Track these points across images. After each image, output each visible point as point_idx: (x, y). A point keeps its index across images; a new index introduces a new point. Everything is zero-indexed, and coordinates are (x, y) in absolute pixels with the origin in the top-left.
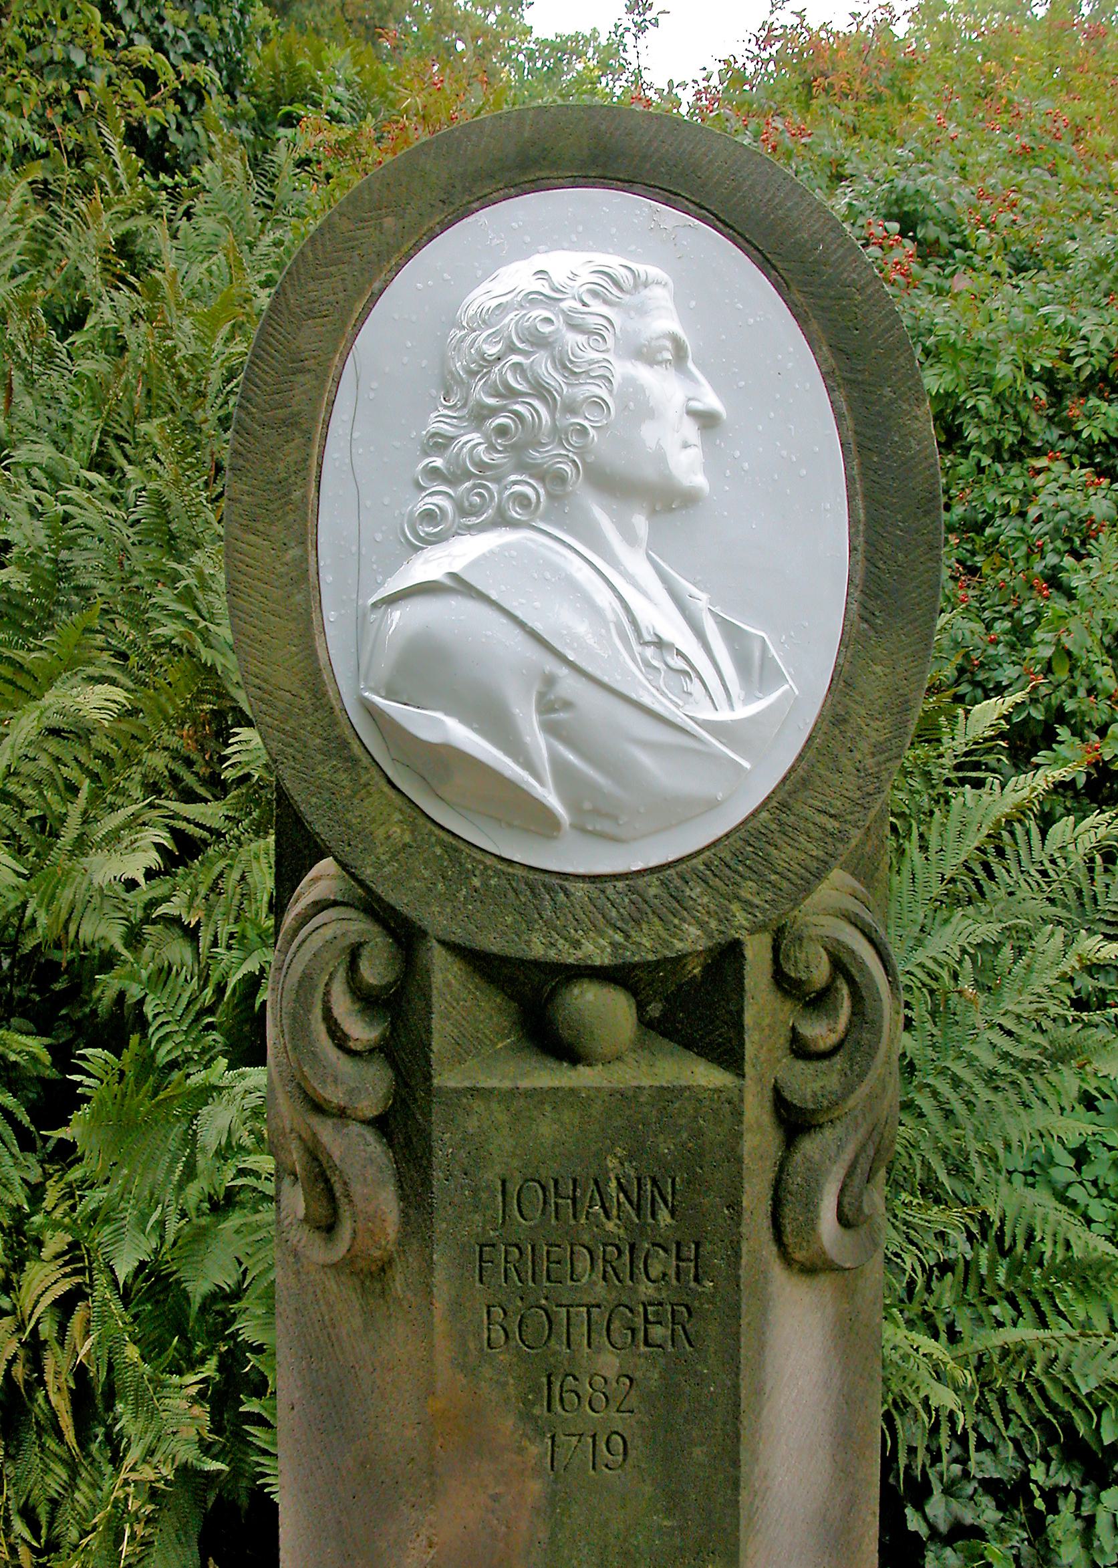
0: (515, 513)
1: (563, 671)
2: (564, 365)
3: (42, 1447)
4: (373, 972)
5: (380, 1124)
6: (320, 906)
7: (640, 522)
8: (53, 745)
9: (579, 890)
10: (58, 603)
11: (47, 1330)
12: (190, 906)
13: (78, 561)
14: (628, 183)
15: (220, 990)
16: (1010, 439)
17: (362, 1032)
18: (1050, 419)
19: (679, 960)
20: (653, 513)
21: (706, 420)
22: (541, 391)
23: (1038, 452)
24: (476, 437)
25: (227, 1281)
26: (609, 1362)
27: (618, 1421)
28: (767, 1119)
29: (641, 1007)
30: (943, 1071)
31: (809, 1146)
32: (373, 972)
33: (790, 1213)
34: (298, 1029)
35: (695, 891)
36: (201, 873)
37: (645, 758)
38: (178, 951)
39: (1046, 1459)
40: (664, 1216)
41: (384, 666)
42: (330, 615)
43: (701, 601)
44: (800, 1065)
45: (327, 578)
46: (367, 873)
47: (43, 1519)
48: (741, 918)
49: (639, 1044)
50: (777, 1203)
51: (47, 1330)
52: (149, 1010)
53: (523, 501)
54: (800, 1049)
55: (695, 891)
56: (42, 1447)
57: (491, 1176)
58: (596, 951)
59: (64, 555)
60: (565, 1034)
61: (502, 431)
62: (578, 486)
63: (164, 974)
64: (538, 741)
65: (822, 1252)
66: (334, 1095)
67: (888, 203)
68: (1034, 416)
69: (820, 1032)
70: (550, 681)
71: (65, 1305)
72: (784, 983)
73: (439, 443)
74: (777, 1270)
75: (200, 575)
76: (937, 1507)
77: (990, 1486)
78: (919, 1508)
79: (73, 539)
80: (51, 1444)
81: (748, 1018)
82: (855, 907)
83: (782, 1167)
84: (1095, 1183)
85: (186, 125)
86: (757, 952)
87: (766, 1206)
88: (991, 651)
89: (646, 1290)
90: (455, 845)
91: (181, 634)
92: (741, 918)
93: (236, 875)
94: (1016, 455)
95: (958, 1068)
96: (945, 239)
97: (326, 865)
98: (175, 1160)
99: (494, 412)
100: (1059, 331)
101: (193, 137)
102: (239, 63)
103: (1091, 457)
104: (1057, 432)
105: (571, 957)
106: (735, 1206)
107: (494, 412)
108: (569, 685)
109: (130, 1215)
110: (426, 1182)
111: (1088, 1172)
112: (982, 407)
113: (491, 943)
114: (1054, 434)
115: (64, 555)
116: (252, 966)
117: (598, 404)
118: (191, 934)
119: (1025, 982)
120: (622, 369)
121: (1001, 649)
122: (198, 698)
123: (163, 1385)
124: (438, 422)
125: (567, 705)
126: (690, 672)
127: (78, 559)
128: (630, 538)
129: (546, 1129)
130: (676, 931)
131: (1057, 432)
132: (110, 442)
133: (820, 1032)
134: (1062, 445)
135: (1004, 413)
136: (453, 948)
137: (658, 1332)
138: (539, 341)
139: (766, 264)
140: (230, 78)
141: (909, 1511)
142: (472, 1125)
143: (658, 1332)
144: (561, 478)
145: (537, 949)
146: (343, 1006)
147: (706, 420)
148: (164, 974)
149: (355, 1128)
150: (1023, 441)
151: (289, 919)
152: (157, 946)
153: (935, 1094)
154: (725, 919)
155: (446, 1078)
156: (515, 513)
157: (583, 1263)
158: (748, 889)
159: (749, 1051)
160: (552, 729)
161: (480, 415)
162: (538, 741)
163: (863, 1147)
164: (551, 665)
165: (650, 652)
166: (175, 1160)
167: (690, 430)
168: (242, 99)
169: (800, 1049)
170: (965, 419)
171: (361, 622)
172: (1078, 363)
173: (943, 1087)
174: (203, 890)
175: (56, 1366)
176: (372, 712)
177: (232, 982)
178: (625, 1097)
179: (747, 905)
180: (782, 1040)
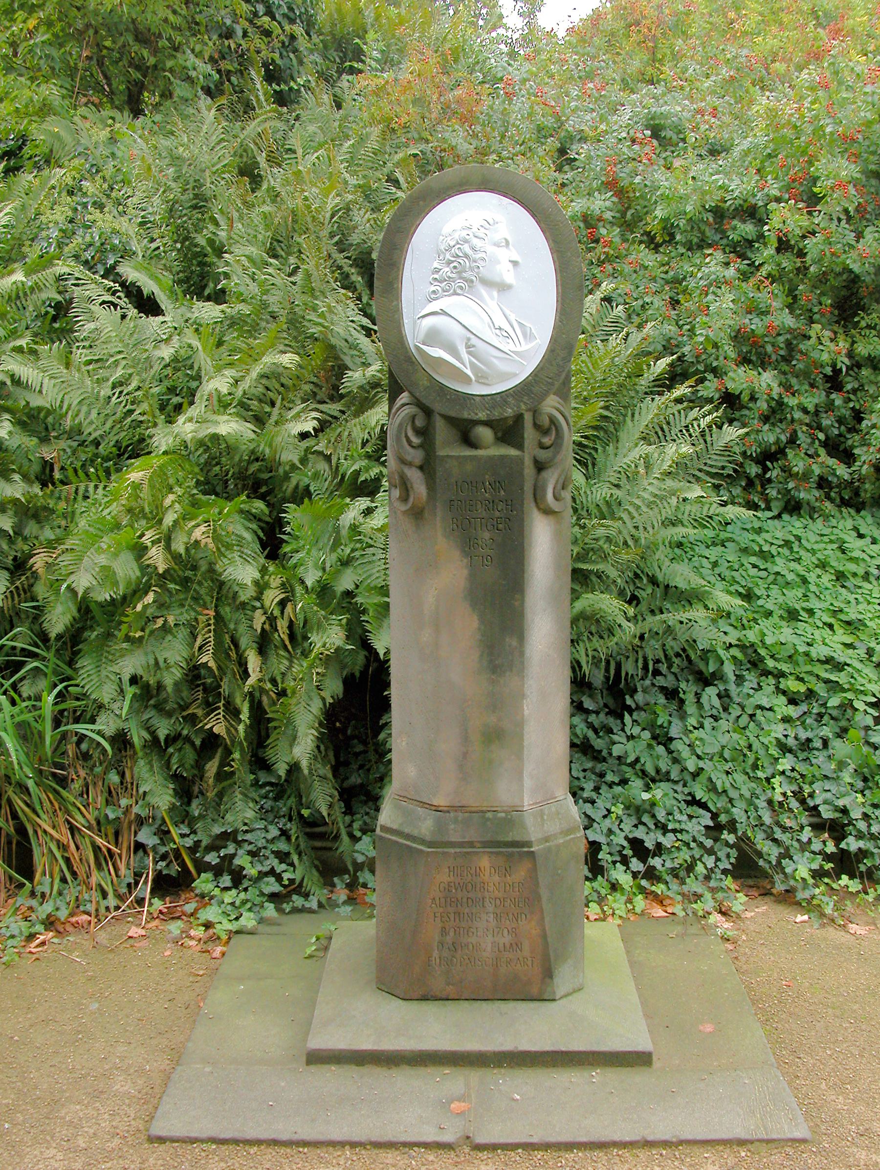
0: (459, 291)
1: (472, 337)
2: (473, 249)
3: (278, 654)
4: (419, 423)
5: (421, 468)
6: (403, 405)
7: (495, 294)
8: (264, 381)
9: (477, 399)
10: (261, 319)
11: (277, 613)
12: (327, 448)
13: (271, 300)
14: (492, 191)
15: (343, 477)
16: (695, 240)
17: (415, 440)
18: (716, 230)
19: (506, 418)
20: (499, 291)
21: (515, 263)
22: (466, 256)
23: (710, 246)
24: (447, 269)
25: (350, 587)
26: (487, 535)
27: (489, 552)
28: (532, 466)
29: (495, 433)
30: (631, 503)
31: (545, 474)
32: (419, 423)
33: (538, 497)
34: (398, 439)
35: (510, 399)
36: (331, 434)
37: (495, 361)
38: (322, 466)
39: (688, 681)
40: (502, 493)
41: (421, 336)
42: (406, 321)
43: (512, 318)
44: (542, 451)
45: (404, 310)
46: (417, 394)
47: (279, 681)
48: (523, 407)
49: (495, 444)
50: (535, 490)
51: (277, 613)
52: (312, 489)
53: (461, 288)
54: (542, 447)
55: (510, 399)
56: (278, 654)
57: (453, 480)
58: (482, 416)
59: (265, 297)
60: (473, 440)
61: (455, 267)
62: (477, 283)
63: (316, 476)
64: (465, 357)
65: (548, 505)
66: (409, 458)
67: (647, 120)
68: (707, 229)
69: (547, 441)
70: (469, 339)
71: (282, 604)
72: (537, 426)
73: (437, 270)
74: (533, 504)
75: (329, 307)
76: (640, 697)
77: (663, 689)
78: (632, 696)
79: (268, 291)
80: (282, 652)
81: (526, 436)
82: (557, 405)
83: (536, 480)
84: (719, 575)
85: (285, 53)
86: (528, 418)
87: (532, 491)
88: (680, 339)
89: (497, 514)
90: (442, 387)
91: (321, 332)
92: (523, 407)
93: (346, 433)
94: (700, 247)
95: (637, 502)
96: (674, 137)
97: (405, 394)
98: (331, 536)
99: (453, 262)
100: (720, 187)
101: (288, 61)
102: (312, 16)
103: (735, 248)
104: (719, 236)
105: (475, 418)
106: (522, 489)
107: (453, 262)
108: (474, 341)
109: (311, 564)
110: (435, 483)
111: (717, 570)
112: (681, 224)
113: (453, 414)
114: (717, 237)
115: (265, 297)
116: (356, 467)
117: (483, 259)
118: (328, 458)
119: (661, 465)
120: (490, 249)
121: (685, 338)
122: (326, 360)
123: (328, 619)
124: (436, 265)
125: (474, 346)
126: (509, 337)
127: (271, 299)
128: (492, 298)
129: (469, 467)
130: (505, 411)
131: (719, 236)
132: (275, 243)
133: (547, 441)
134: (722, 242)
135: (692, 228)
136: (443, 416)
137: (500, 526)
138: (466, 241)
139: (533, 216)
140: (308, 25)
141: (627, 697)
142: (447, 466)
143: (500, 526)
144: (472, 281)
145: (466, 415)
146: (410, 433)
147: (515, 263)
148: (316, 476)
149: (414, 469)
150: (702, 240)
151: (393, 411)
152: (314, 463)
153: (629, 513)
154: (519, 407)
155: (441, 453)
156: (459, 291)
157: (479, 506)
158: (525, 399)
159: (526, 445)
160: (469, 353)
161: (449, 263)
162: (465, 357)
163: (560, 475)
164: (469, 335)
165: (498, 331)
166: (331, 536)
167: (510, 266)
168: (314, 37)
169: (542, 447)
170: (676, 230)
171: (415, 323)
172: (729, 203)
173: (631, 509)
174: (333, 440)
175: (282, 625)
176: (417, 348)
177: (349, 473)
178: (491, 458)
179: (525, 403)
180: (536, 443)
